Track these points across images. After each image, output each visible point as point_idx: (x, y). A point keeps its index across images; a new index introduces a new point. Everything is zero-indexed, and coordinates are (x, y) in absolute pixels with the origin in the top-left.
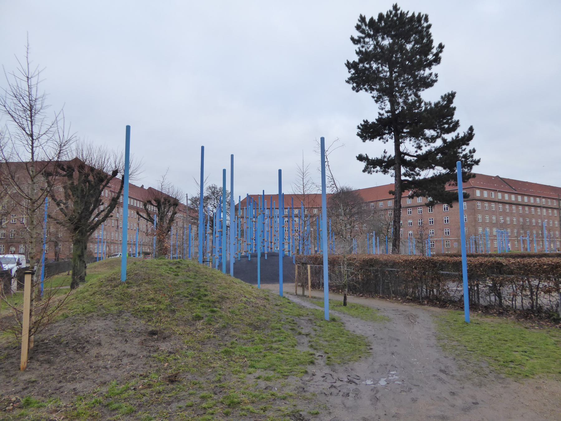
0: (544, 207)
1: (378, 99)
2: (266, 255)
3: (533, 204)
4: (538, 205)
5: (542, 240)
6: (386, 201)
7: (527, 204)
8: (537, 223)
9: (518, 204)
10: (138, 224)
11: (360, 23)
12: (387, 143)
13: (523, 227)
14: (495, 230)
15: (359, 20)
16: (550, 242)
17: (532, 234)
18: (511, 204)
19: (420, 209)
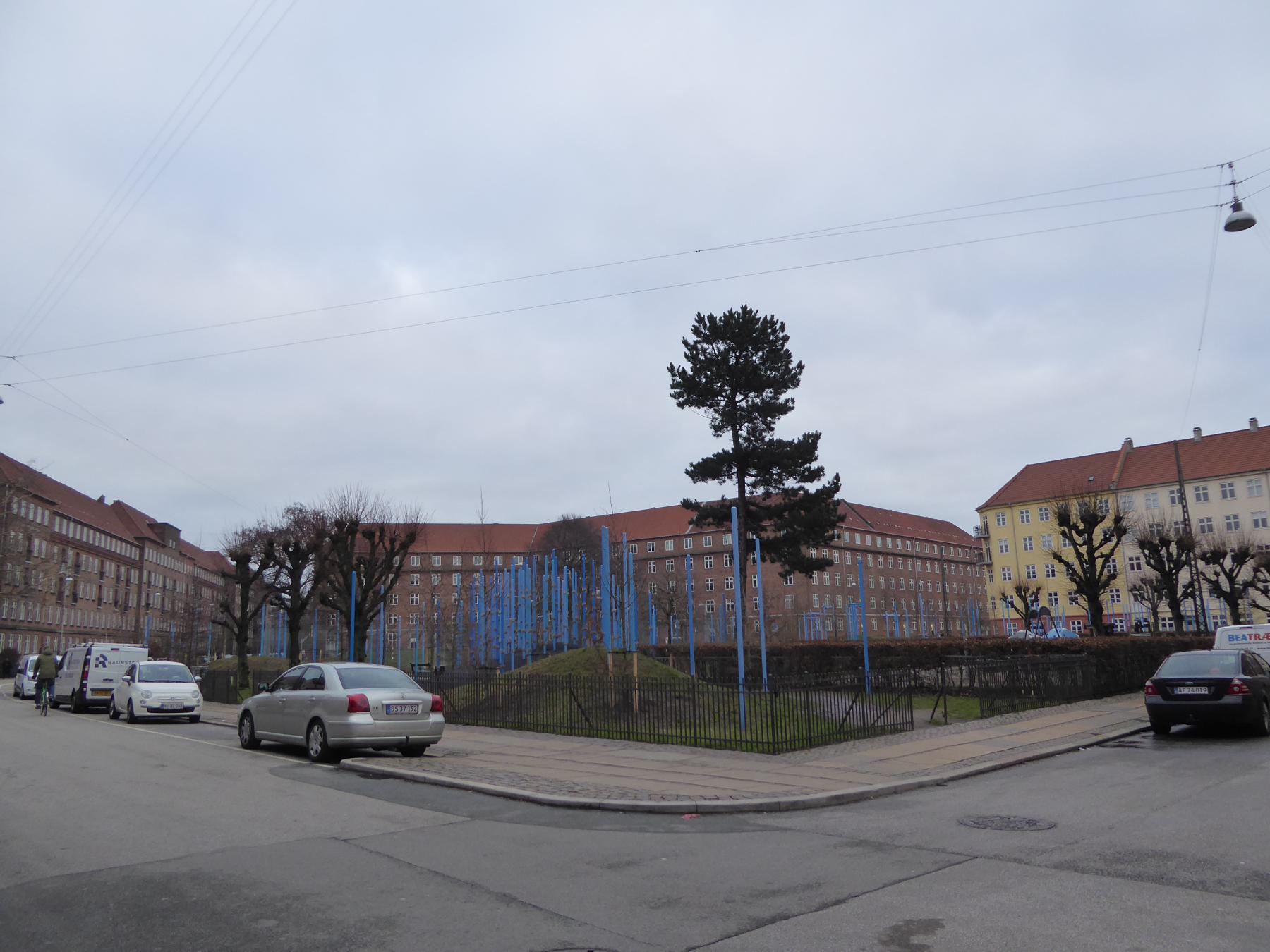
0: (919, 558)
1: (717, 429)
2: (545, 647)
3: (901, 553)
4: (909, 554)
5: (917, 618)
6: (645, 542)
7: (891, 551)
8: (907, 585)
9: (876, 553)
10: (100, 586)
11: (697, 324)
12: (723, 484)
13: (885, 594)
14: (839, 599)
15: (696, 320)
16: (929, 620)
17: (899, 606)
18: (865, 551)
19: (709, 560)
